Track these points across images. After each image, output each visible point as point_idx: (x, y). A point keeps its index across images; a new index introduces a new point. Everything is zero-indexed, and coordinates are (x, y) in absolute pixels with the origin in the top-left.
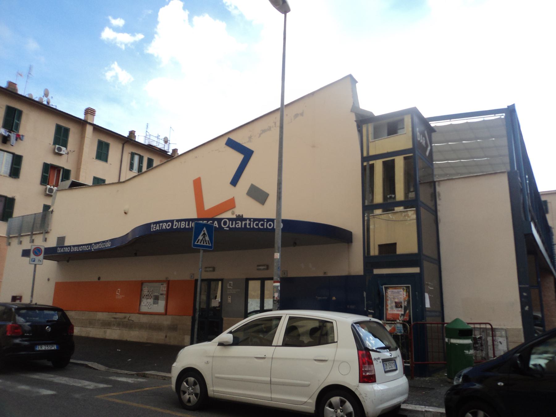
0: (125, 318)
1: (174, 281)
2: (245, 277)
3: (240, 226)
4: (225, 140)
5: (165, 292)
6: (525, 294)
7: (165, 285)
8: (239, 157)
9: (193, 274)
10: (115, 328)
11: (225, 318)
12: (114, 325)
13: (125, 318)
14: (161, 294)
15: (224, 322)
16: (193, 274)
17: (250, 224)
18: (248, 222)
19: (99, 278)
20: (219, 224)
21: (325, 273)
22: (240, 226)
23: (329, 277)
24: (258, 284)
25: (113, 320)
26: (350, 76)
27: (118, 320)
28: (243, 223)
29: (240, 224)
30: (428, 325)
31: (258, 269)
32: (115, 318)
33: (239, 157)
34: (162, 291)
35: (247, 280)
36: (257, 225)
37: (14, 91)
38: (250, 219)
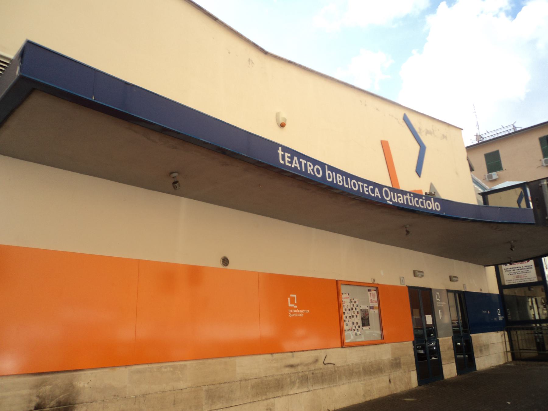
0: (317, 361)
1: (384, 286)
5: (376, 305)
6: (492, 349)
7: (347, 341)
8: (490, 197)
10: (295, 390)
12: (293, 383)
13: (317, 361)
14: (372, 308)
17: (411, 199)
19: (225, 261)
25: (287, 371)
26: (451, 280)
27: (300, 369)
32: (292, 366)
33: (490, 197)
34: (372, 302)
36: (417, 202)
37: (420, 194)
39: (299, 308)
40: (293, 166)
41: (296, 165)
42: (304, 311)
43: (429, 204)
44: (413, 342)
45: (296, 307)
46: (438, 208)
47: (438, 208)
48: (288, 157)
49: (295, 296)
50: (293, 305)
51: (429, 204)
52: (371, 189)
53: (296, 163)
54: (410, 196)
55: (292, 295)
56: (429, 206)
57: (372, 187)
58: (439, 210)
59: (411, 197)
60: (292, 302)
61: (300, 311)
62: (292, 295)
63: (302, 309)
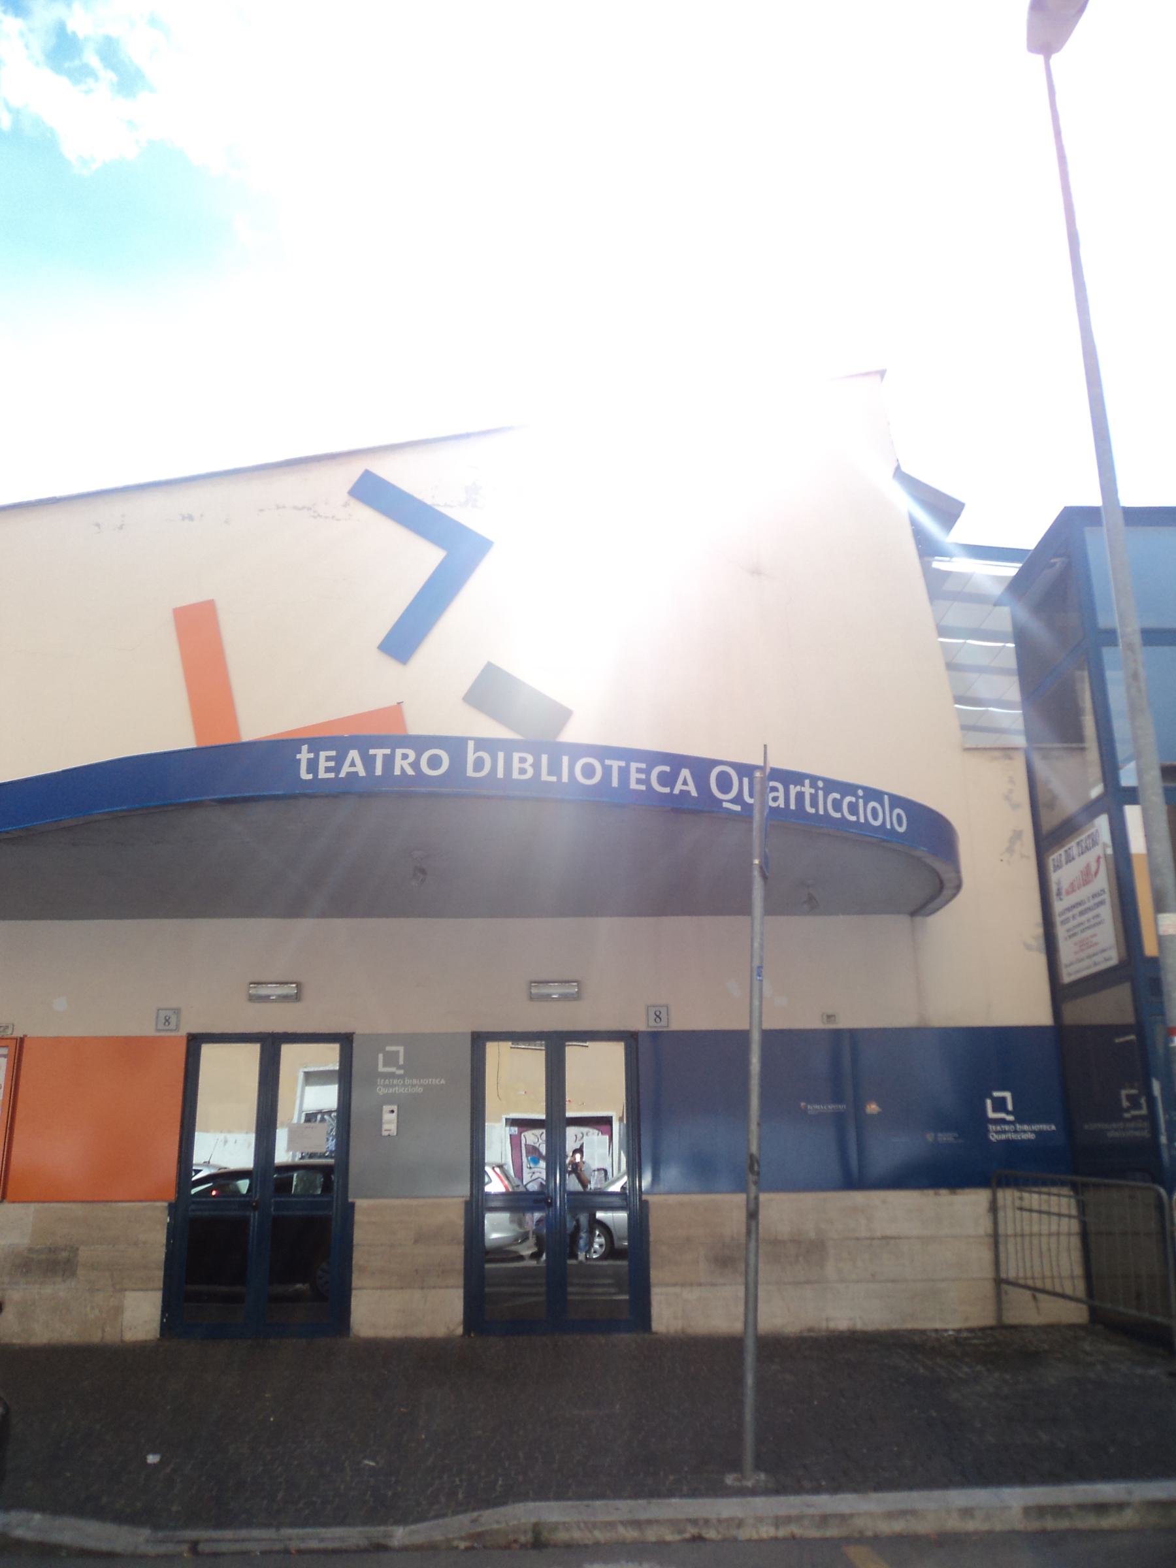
2: (468, 1027)
3: (781, 803)
4: (352, 473)
9: (177, 1011)
11: (361, 1204)
15: (358, 1217)
16: (177, 1011)
17: (814, 798)
18: (808, 790)
20: (701, 779)
21: (830, 1017)
22: (781, 803)
23: (673, 1032)
24: (534, 1060)
28: (793, 790)
29: (781, 794)
30: (283, 1155)
31: (253, 999)
35: (479, 1040)
36: (837, 805)
38: (814, 780)
39: (1020, 1120)
40: (676, 791)
41: (685, 788)
42: (1036, 1127)
43: (874, 810)
44: (170, 1205)
45: (1010, 1118)
46: (900, 824)
47: (900, 824)
48: (639, 770)
49: (1008, 1095)
50: (393, 1069)
51: (874, 810)
52: (834, 800)
53: (685, 783)
54: (813, 784)
55: (996, 1094)
56: (875, 817)
57: (838, 796)
58: (902, 830)
59: (817, 788)
60: (1000, 1105)
61: (1026, 1127)
62: (996, 1094)
63: (1030, 1122)
